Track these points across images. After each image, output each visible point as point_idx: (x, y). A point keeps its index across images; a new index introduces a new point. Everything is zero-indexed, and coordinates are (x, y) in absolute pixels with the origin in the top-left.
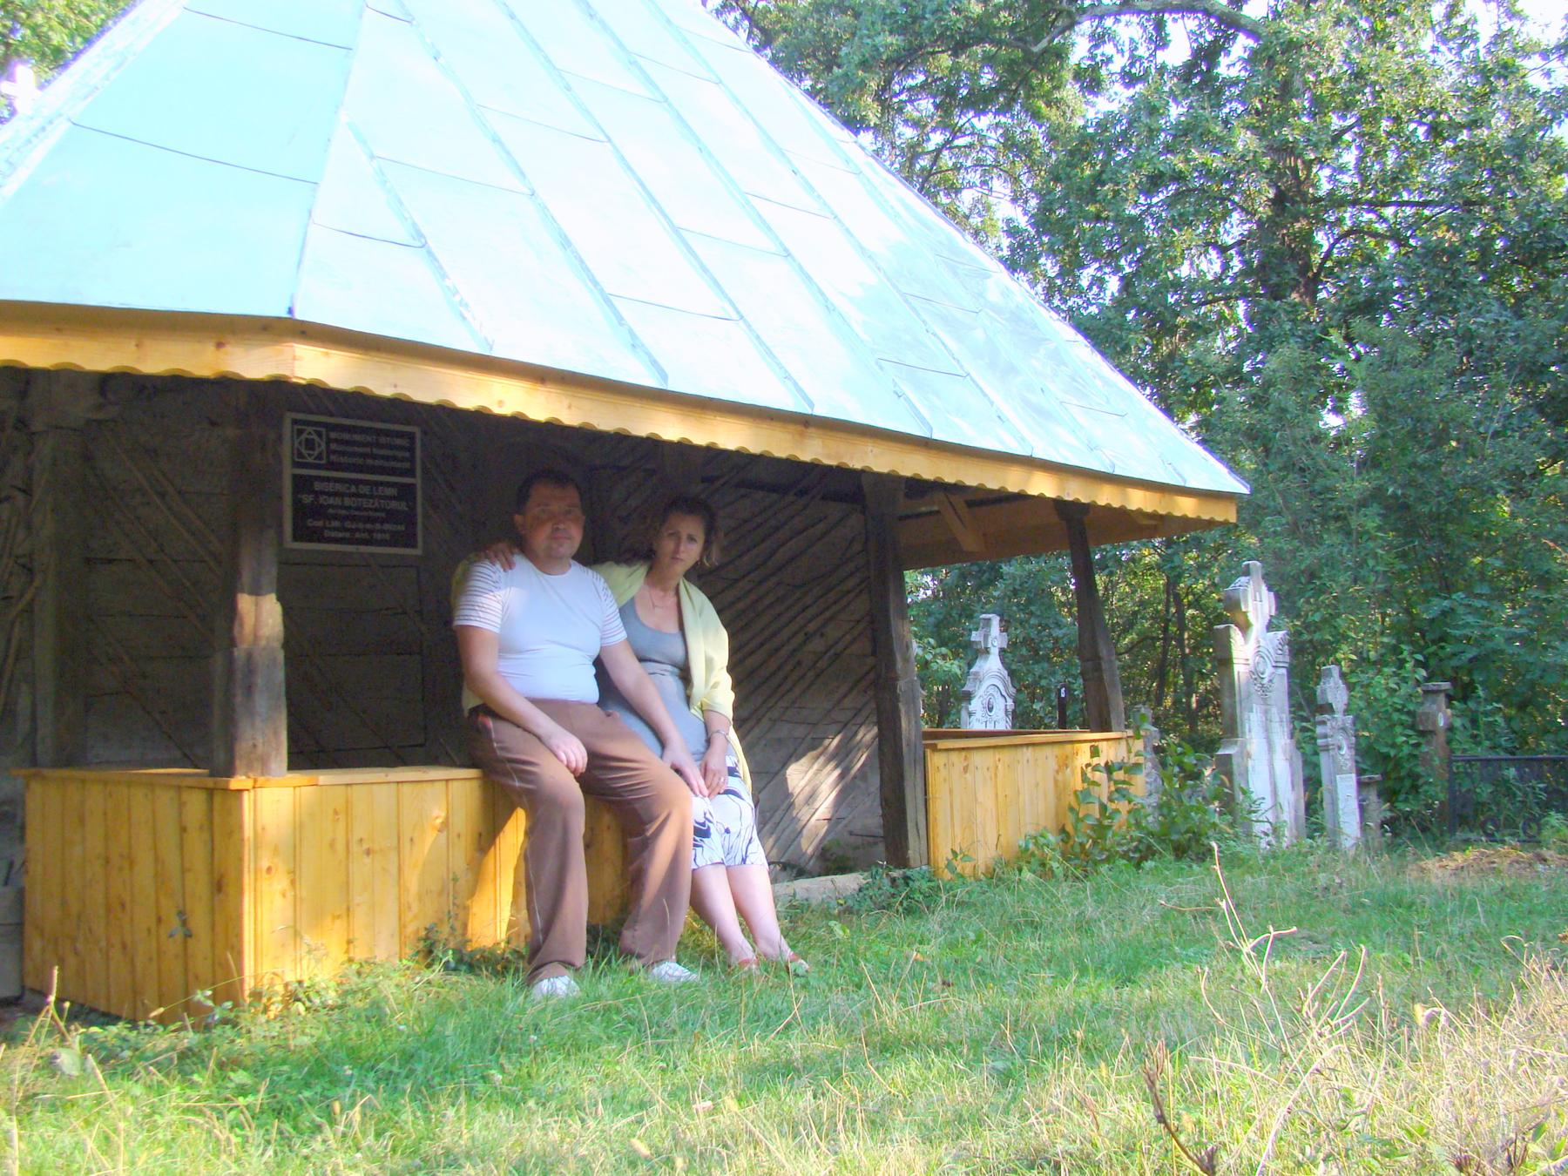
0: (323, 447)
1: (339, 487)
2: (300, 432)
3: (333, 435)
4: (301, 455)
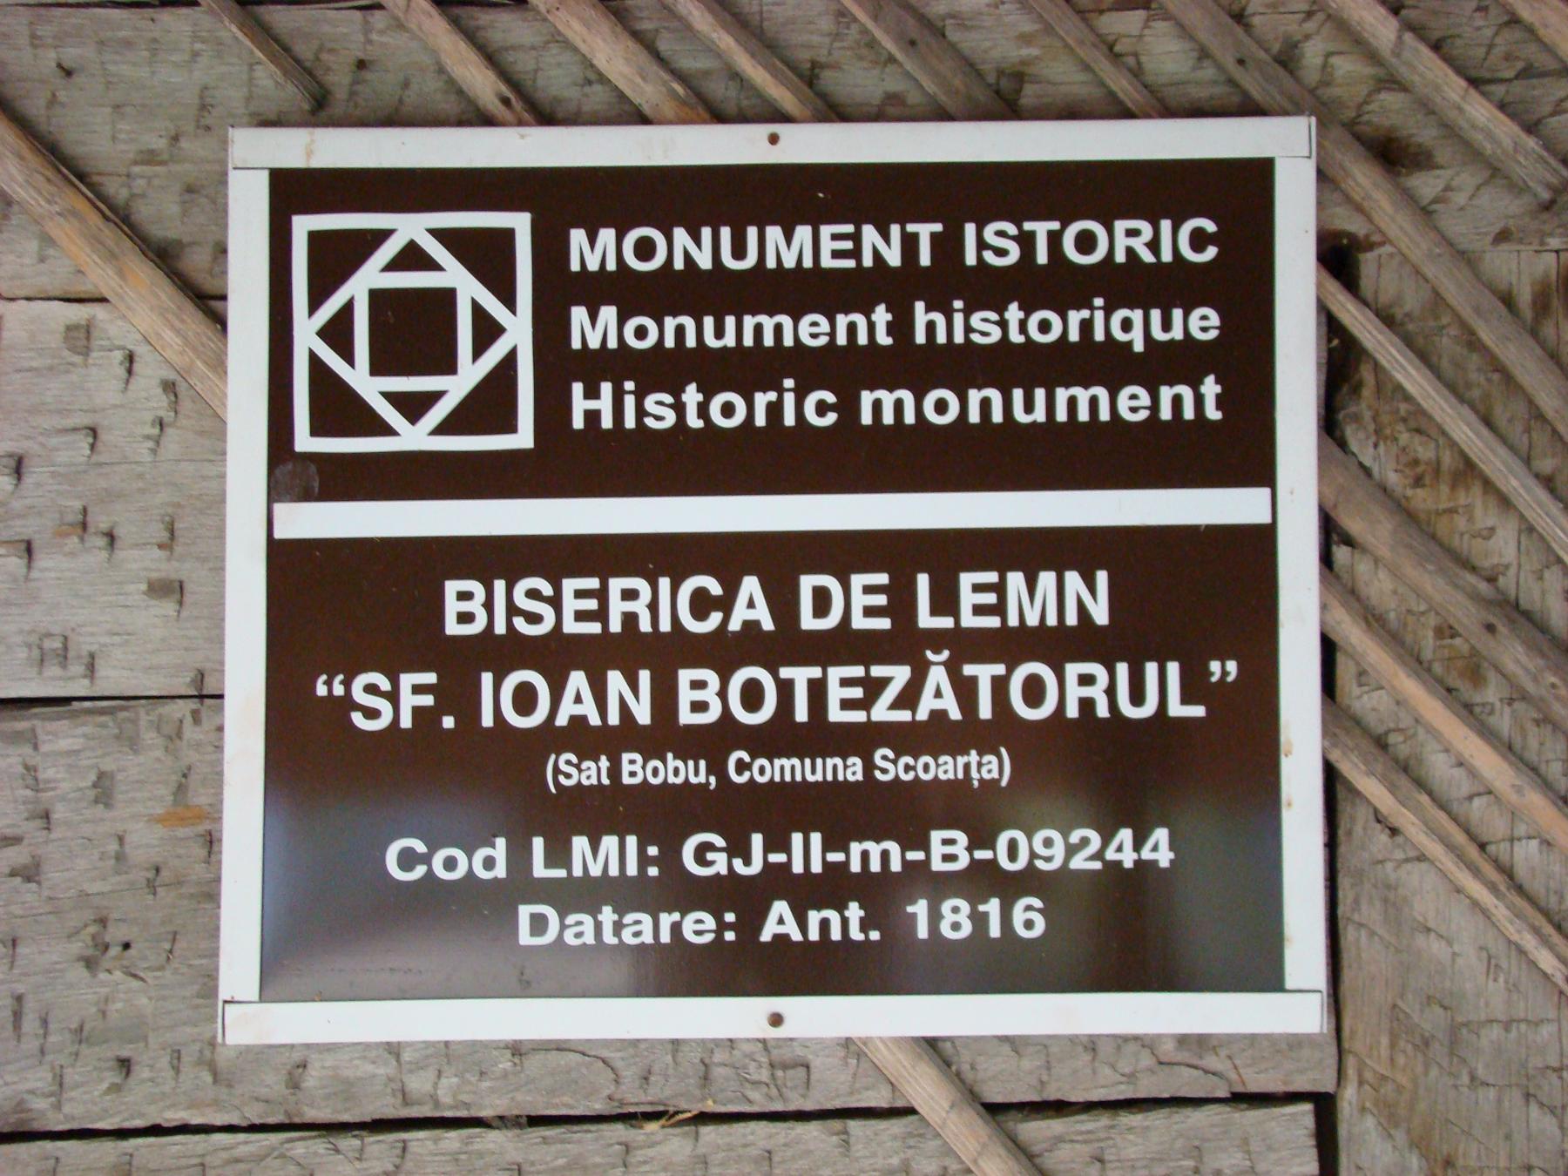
0: (518, 331)
1: (570, 607)
2: (336, 258)
3: (590, 251)
4: (338, 408)
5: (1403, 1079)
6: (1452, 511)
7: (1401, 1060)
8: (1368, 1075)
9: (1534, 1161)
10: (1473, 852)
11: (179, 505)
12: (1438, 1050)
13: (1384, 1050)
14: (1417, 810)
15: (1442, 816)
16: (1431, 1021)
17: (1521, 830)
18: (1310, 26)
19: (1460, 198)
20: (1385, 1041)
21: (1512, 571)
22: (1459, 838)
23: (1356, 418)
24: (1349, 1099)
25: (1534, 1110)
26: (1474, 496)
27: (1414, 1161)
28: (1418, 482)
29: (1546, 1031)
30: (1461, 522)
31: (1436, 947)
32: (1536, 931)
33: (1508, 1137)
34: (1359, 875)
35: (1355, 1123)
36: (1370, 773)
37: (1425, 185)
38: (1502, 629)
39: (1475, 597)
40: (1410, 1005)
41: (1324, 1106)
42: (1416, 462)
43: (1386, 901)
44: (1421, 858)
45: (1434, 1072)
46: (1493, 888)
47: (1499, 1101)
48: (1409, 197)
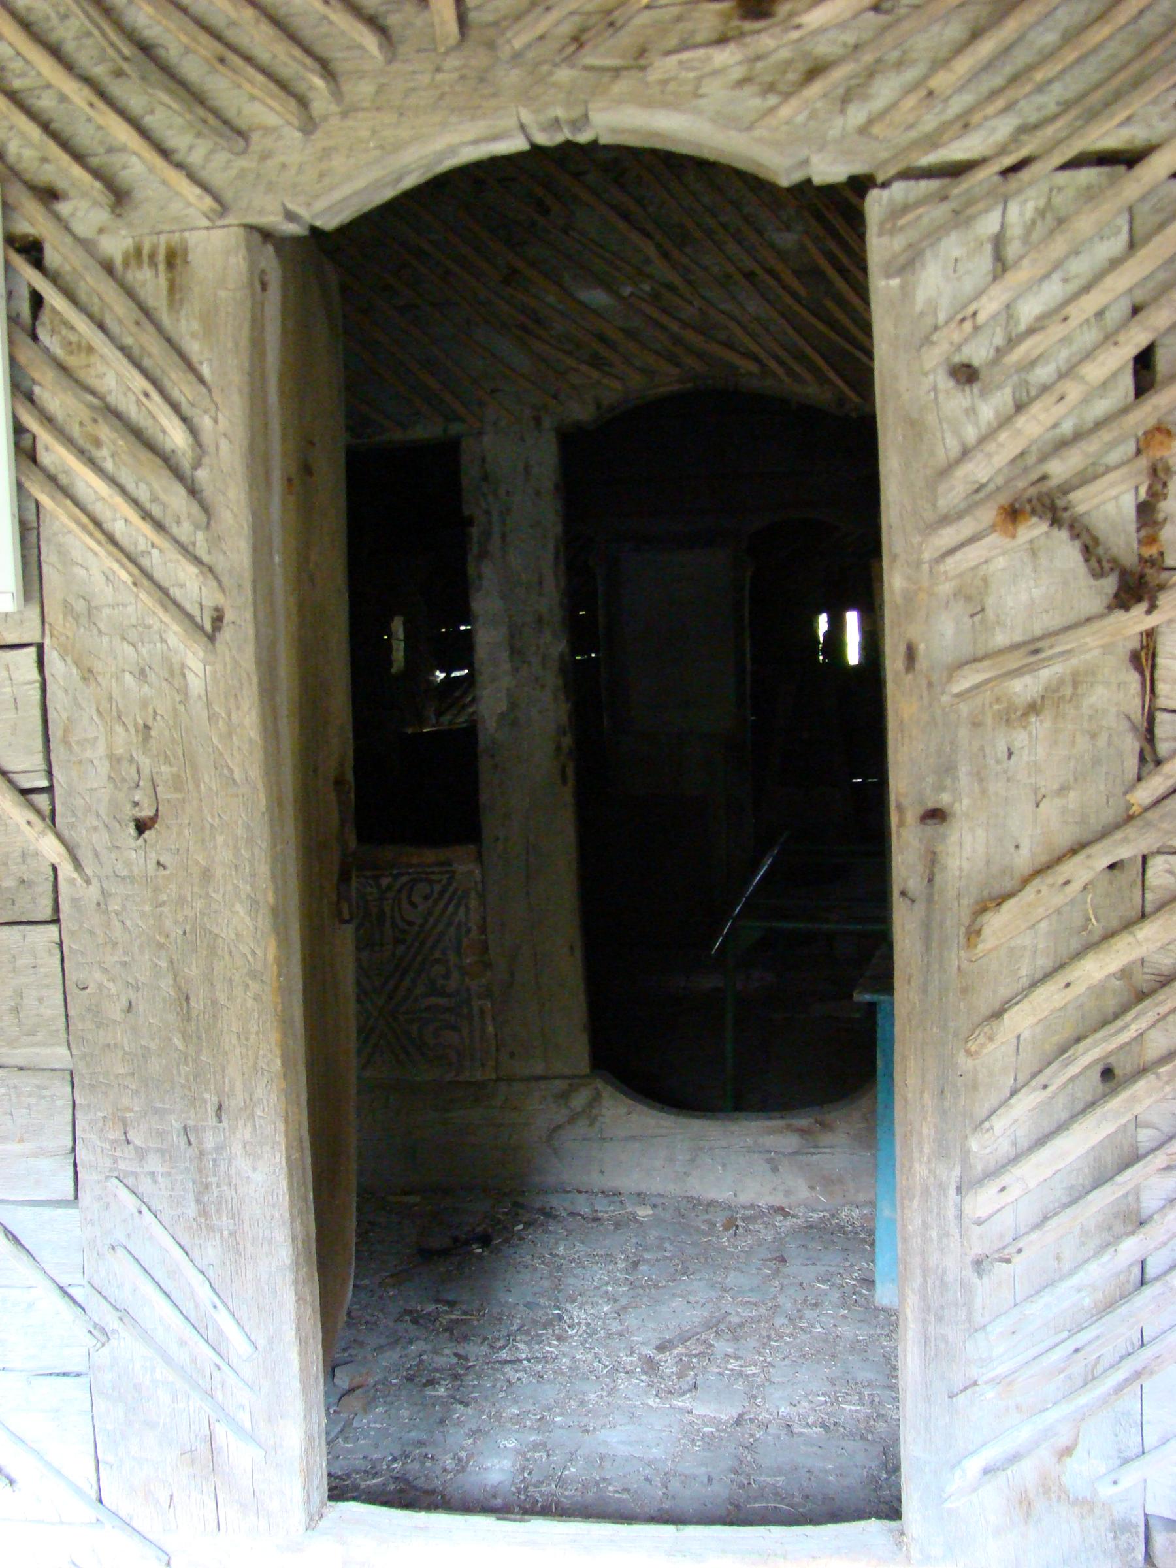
5: (70, 634)
6: (88, 366)
7: (68, 625)
8: (56, 633)
9: (126, 667)
10: (91, 526)
11: (1012, 627)
12: (84, 620)
13: (61, 621)
14: (65, 508)
15: (77, 511)
16: (80, 606)
17: (118, 515)
18: (11, 134)
19: (80, 214)
20: (61, 617)
21: (113, 394)
22: (85, 520)
23: (43, 324)
24: (47, 642)
25: (126, 645)
26: (1118, 244)
27: (74, 670)
28: (71, 353)
29: (131, 609)
30: (93, 372)
31: (82, 572)
32: (118, 561)
33: (115, 658)
34: (48, 541)
35: (51, 656)
36: (43, 492)
37: (64, 208)
38: (100, 420)
39: (91, 407)
40: (72, 600)
41: (40, 648)
42: (70, 343)
43: (59, 552)
44: (70, 532)
45: (82, 630)
46: (99, 542)
47: (111, 641)
48: (58, 217)
